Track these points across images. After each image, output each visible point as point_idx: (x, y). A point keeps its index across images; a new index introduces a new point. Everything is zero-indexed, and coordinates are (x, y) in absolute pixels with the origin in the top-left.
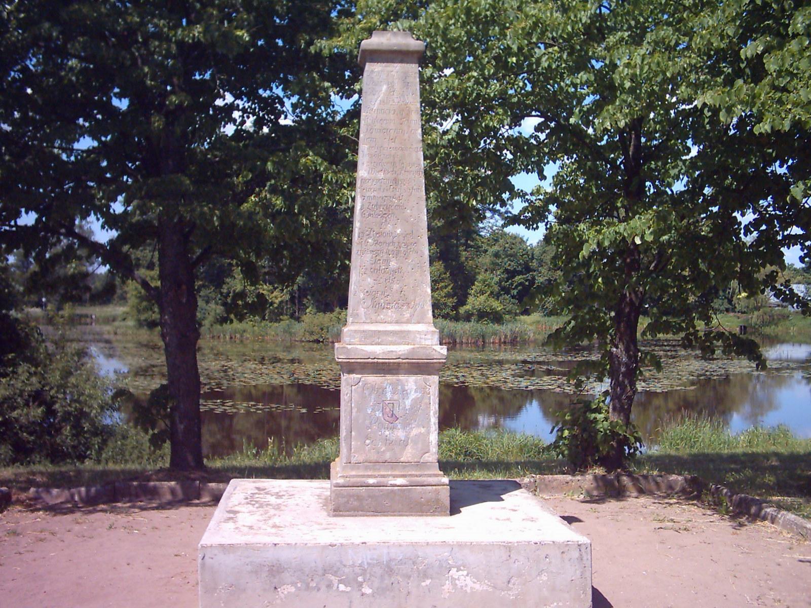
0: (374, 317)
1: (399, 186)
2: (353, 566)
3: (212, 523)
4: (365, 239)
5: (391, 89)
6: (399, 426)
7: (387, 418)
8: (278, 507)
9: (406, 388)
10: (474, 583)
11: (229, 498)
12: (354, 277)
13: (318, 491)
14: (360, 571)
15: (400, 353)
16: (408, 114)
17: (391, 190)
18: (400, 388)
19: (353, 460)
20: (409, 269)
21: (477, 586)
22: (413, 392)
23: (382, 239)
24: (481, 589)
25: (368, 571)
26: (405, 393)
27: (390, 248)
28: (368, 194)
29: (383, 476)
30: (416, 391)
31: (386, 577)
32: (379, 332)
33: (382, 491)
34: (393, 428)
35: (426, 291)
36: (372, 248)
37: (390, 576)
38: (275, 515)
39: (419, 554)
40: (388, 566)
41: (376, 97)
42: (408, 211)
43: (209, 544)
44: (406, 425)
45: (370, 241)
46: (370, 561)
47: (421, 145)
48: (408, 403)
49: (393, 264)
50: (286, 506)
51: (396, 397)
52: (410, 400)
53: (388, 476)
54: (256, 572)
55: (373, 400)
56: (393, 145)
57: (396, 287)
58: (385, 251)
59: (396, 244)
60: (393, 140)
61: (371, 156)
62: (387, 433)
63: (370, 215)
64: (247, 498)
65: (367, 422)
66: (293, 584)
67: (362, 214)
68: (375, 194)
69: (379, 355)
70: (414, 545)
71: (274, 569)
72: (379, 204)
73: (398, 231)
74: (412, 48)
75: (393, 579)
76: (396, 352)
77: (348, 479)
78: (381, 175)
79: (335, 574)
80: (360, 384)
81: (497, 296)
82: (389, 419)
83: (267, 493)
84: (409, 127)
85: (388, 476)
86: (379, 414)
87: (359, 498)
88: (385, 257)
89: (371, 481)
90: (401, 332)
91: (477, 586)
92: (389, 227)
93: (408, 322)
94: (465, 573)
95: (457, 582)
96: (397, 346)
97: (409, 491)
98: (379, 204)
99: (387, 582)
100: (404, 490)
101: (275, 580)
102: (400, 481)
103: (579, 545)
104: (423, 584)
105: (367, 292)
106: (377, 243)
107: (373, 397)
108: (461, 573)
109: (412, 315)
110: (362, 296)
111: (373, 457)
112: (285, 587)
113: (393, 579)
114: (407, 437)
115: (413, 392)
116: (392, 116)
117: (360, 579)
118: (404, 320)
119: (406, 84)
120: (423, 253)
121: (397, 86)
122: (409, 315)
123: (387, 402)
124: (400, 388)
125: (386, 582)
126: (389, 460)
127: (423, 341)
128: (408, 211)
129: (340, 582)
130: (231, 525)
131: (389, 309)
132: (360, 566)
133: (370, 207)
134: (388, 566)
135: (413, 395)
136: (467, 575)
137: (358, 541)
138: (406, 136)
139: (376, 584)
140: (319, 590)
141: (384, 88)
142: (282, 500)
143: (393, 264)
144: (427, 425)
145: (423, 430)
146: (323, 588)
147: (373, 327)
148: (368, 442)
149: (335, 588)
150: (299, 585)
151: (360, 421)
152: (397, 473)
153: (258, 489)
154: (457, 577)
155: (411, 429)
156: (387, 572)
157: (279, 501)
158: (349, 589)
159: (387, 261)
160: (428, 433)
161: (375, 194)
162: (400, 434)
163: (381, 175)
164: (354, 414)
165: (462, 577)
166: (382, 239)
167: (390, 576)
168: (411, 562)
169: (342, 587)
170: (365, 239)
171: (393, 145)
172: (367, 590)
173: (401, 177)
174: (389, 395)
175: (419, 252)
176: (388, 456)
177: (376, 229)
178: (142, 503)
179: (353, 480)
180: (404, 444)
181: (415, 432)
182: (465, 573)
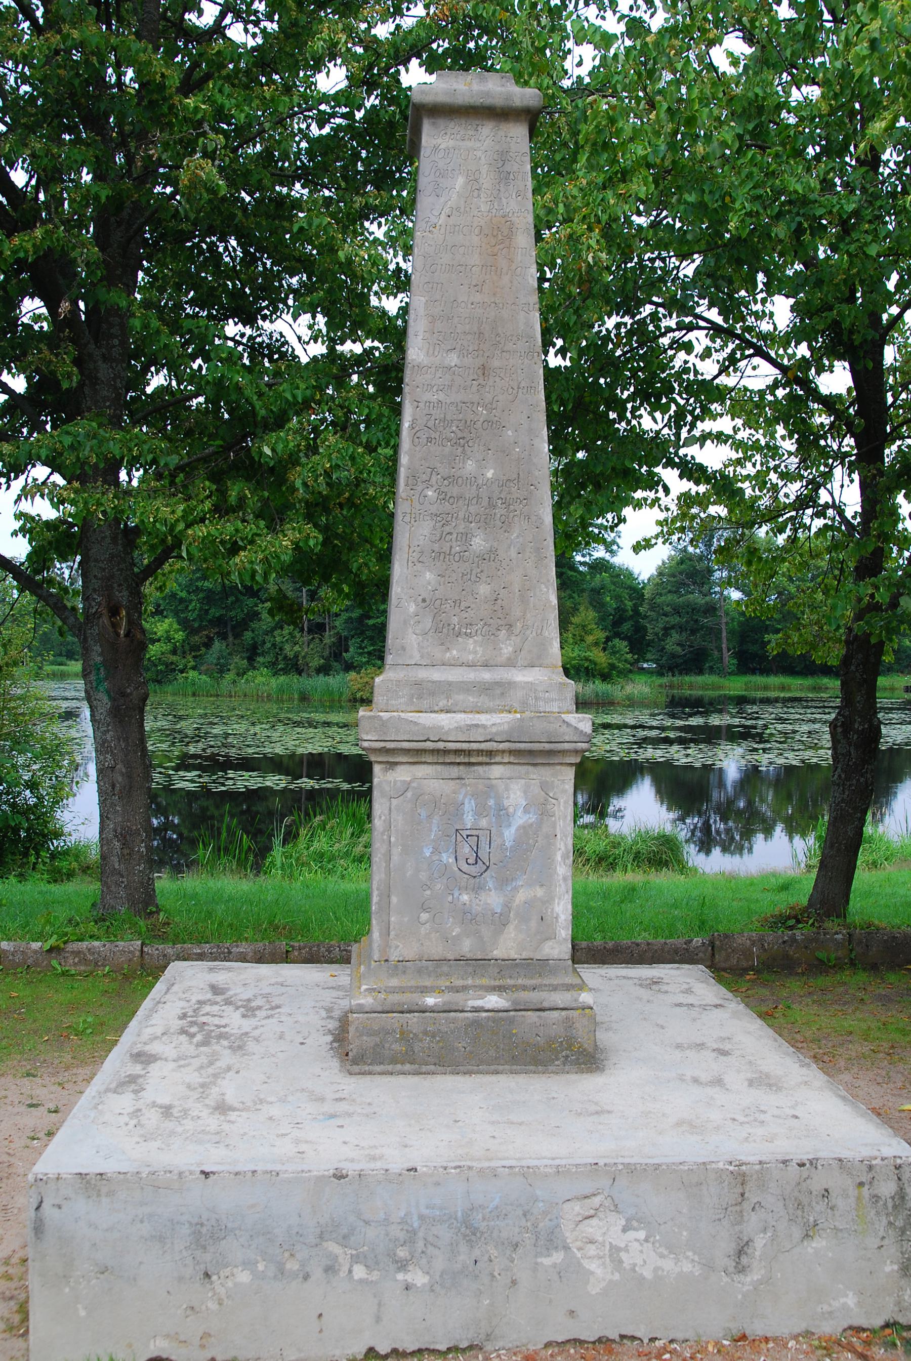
0: (438, 653)
1: (491, 383)
2: (386, 1222)
3: (92, 1090)
4: (420, 488)
5: (473, 180)
6: (490, 884)
7: (465, 867)
8: (239, 1046)
9: (506, 803)
10: (662, 1256)
11: (154, 1010)
12: (399, 570)
13: (328, 997)
14: (402, 1236)
15: (494, 730)
16: (510, 236)
17: (474, 388)
18: (491, 802)
19: (394, 956)
20: (513, 553)
21: (668, 1265)
22: (519, 813)
23: (455, 491)
24: (677, 1270)
25: (421, 1234)
26: (502, 814)
27: (472, 509)
28: (427, 396)
29: (456, 989)
30: (526, 810)
31: (463, 1248)
32: (450, 684)
33: (454, 1021)
34: (478, 889)
35: (548, 600)
36: (434, 509)
37: (471, 1244)
38: (229, 1069)
39: (539, 1193)
40: (466, 1223)
41: (442, 200)
42: (510, 433)
43: (52, 1171)
44: (503, 882)
45: (430, 493)
46: (426, 1212)
47: (535, 298)
48: (509, 834)
49: (479, 543)
50: (257, 1040)
51: (484, 823)
52: (513, 830)
53: (465, 988)
54: (161, 1239)
55: (435, 829)
56: (478, 297)
57: (484, 589)
58: (461, 515)
59: (485, 502)
60: (478, 287)
61: (433, 320)
62: (465, 898)
63: (429, 440)
64: (184, 1016)
65: (423, 876)
66: (248, 1264)
67: (415, 436)
68: (441, 396)
69: (447, 733)
70: (527, 1173)
71: (204, 1230)
72: (448, 418)
73: (490, 474)
74: (518, 102)
75: (477, 1253)
76: (484, 727)
77: (382, 996)
78: (453, 359)
79: (344, 1240)
80: (409, 794)
81: (207, 733)
82: (473, 870)
83: (228, 1002)
84: (511, 260)
85: (465, 988)
86: (447, 858)
87: (405, 1035)
88: (461, 529)
89: (430, 1001)
90: (498, 684)
91: (668, 1265)
92: (470, 466)
93: (510, 663)
94: (642, 1235)
95: (623, 1255)
96: (488, 716)
97: (512, 1021)
98: (448, 418)
99: (464, 1256)
100: (501, 1019)
101: (208, 1257)
102: (493, 1001)
103: (898, 1167)
104: (546, 1261)
105: (424, 600)
106: (443, 497)
107: (436, 820)
108: (631, 1235)
109: (518, 651)
110: (412, 608)
111: (436, 949)
112: (227, 1271)
113: (477, 1253)
114: (507, 906)
115: (519, 813)
116: (476, 240)
117: (402, 1253)
118: (502, 659)
119: (504, 177)
120: (540, 518)
121: (487, 181)
122: (510, 649)
123: (465, 833)
124: (491, 802)
125: (462, 1257)
126: (469, 956)
127: (541, 703)
128: (510, 433)
129: (355, 1259)
130: (125, 1101)
131: (469, 635)
132: (403, 1221)
133: (430, 424)
134: (466, 1223)
135: (520, 819)
136: (646, 1240)
137: (397, 1162)
138: (506, 279)
139: (439, 1263)
140: (306, 1277)
141: (461, 181)
142: (253, 1022)
143: (479, 543)
144: (545, 878)
145: (540, 892)
146: (317, 1273)
147: (437, 675)
148: (424, 916)
149: (343, 1274)
150: (261, 1267)
151: (409, 874)
152: (485, 981)
153: (215, 989)
154: (622, 1245)
155: (516, 889)
156: (465, 1236)
157: (247, 1025)
158: (375, 1276)
159: (466, 537)
160: (549, 900)
161: (441, 396)
162: (493, 900)
163: (453, 359)
164: (395, 858)
165: (636, 1244)
166: (455, 491)
167: (471, 1244)
168: (520, 1212)
169: (359, 1272)
170: (420, 488)
171: (478, 297)
172: (419, 1279)
173: (496, 363)
174: (469, 820)
175: (533, 518)
176: (467, 947)
177: (444, 470)
178: (96, 943)
179: (395, 998)
180: (501, 921)
181: (521, 896)
182: (642, 1235)
